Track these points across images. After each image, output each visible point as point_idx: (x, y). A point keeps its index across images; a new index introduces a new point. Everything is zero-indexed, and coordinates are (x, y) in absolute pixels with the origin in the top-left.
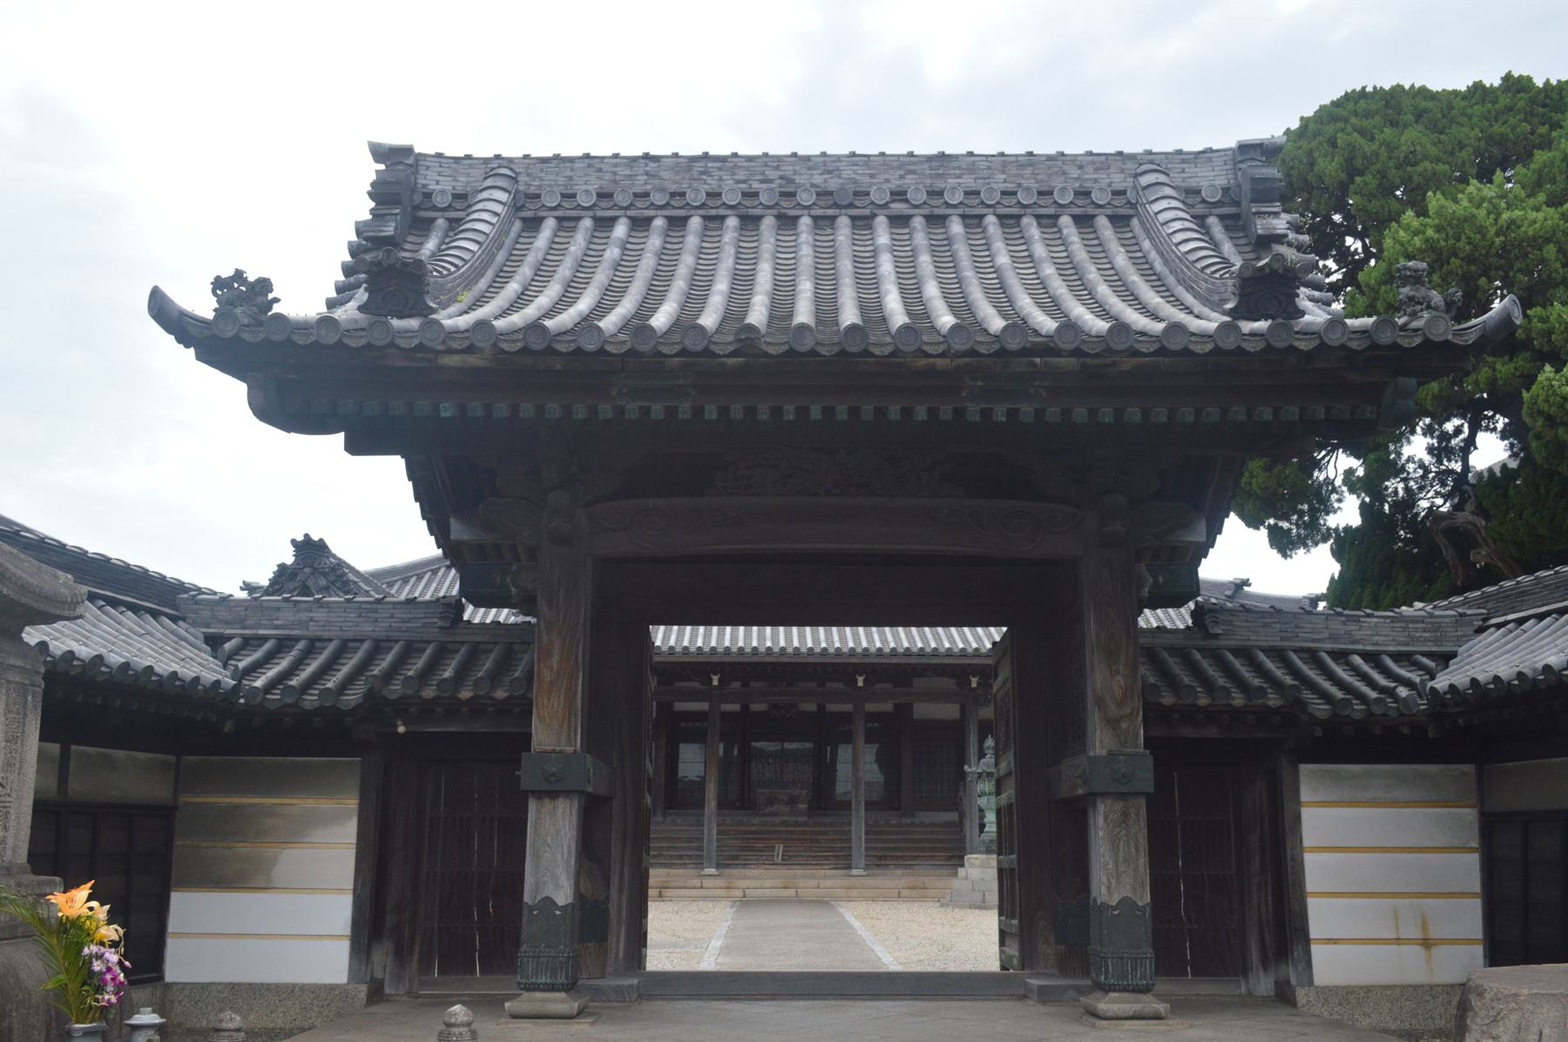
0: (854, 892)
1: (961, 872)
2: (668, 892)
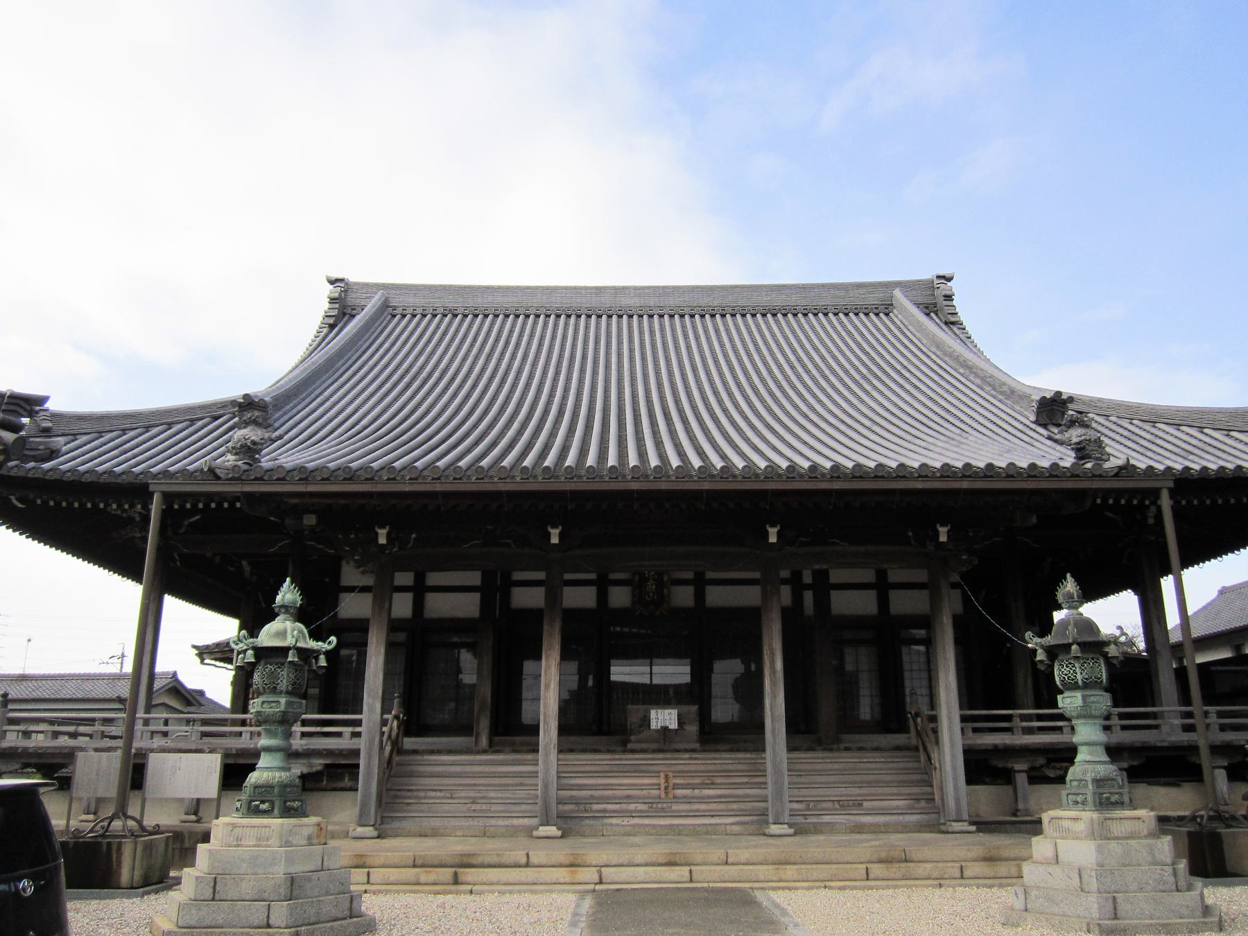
0: (790, 871)
1: (1040, 846)
2: (469, 874)
